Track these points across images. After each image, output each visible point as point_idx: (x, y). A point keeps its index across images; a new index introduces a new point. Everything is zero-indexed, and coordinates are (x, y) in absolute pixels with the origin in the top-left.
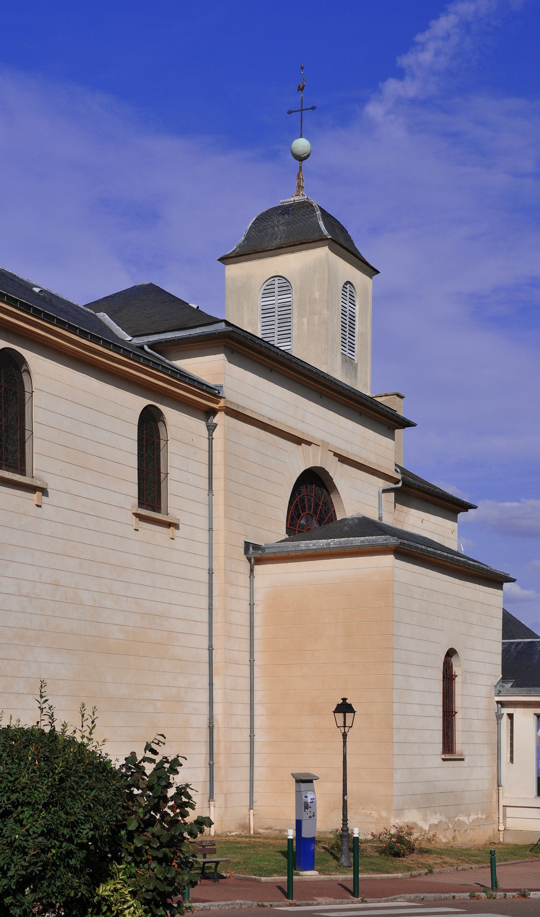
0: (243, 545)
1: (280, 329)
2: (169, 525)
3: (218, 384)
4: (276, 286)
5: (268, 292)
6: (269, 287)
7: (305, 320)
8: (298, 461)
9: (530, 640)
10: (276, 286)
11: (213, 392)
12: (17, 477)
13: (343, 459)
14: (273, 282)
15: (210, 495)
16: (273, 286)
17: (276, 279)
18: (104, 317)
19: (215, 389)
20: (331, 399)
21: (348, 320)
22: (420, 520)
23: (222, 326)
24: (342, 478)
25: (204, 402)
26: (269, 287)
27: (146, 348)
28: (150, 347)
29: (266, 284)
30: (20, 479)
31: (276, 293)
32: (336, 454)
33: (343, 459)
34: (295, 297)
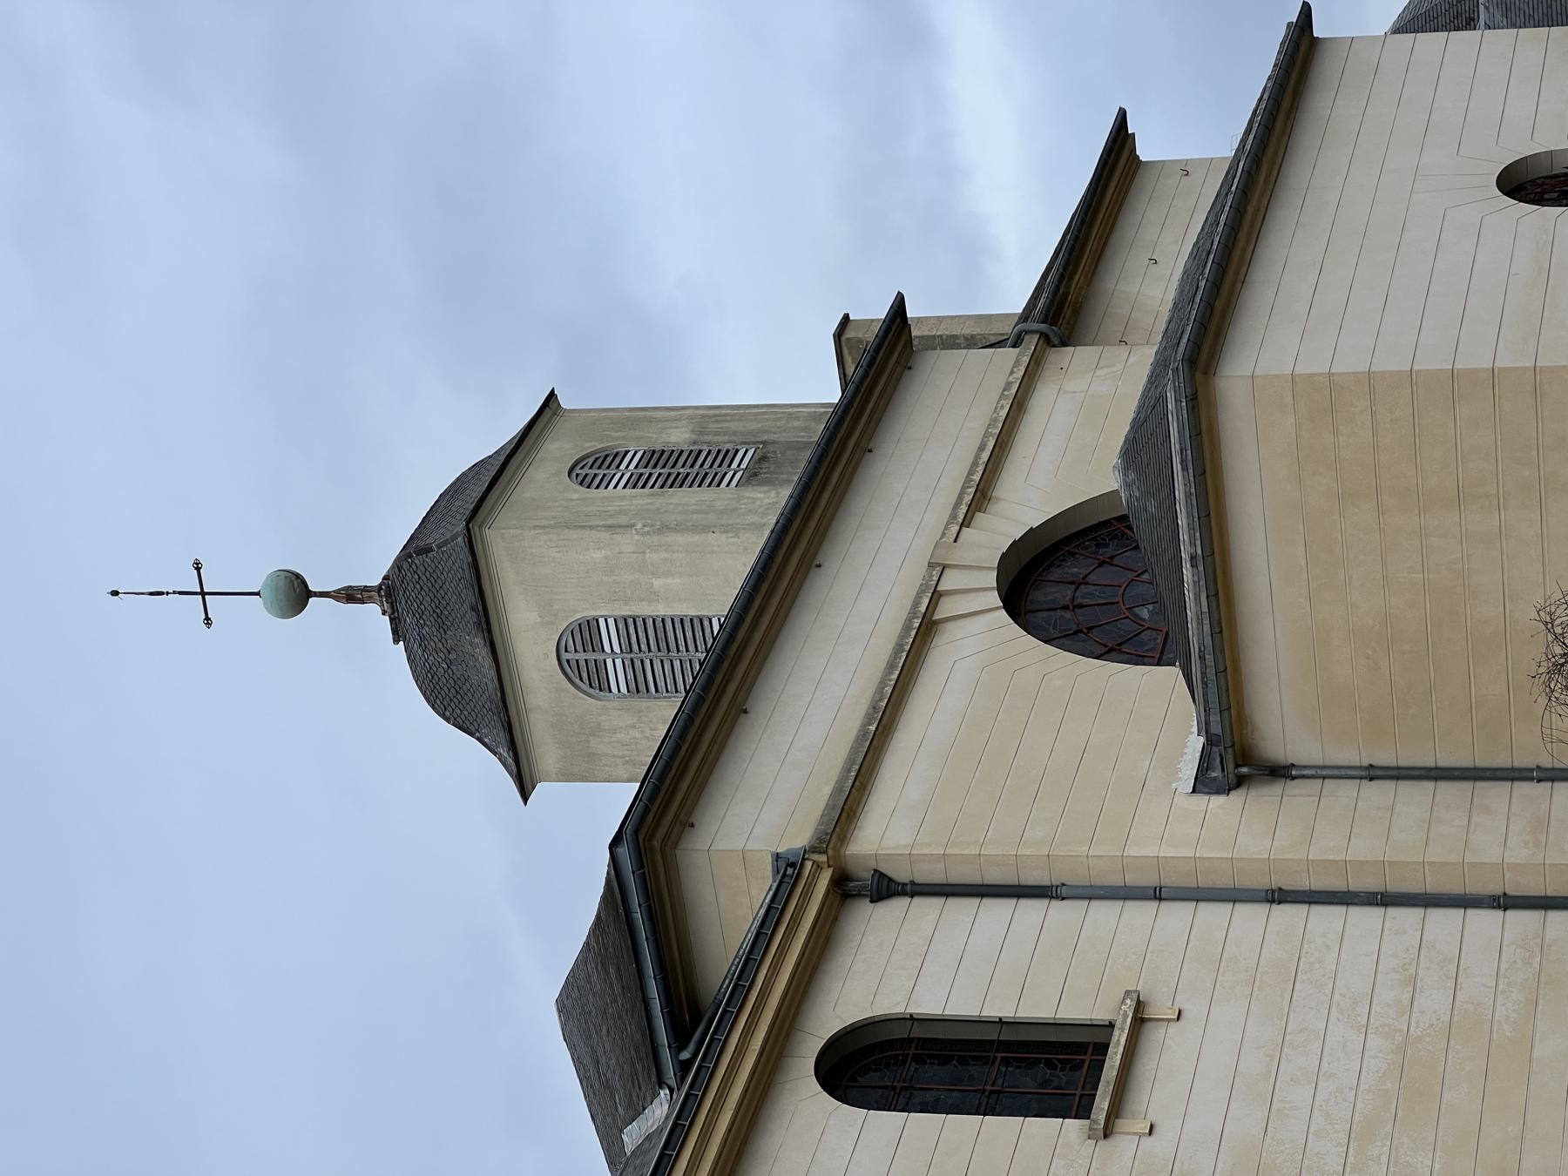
0: (1201, 800)
1: (682, 648)
2: (1140, 1021)
3: (770, 868)
4: (581, 656)
5: (593, 679)
6: (585, 675)
7: (658, 583)
8: (982, 636)
9: (1177, 467)
10: (581, 656)
11: (789, 870)
12: (1120, 1039)
13: (980, 496)
14: (573, 664)
15: (1064, 891)
16: (582, 664)
17: (565, 656)
18: (632, 1136)
19: (784, 875)
20: (822, 535)
21: (658, 471)
22: (1153, 268)
23: (623, 851)
24: (1033, 498)
25: (835, 884)
26: (585, 675)
27: (685, 1055)
28: (681, 1048)
29: (577, 681)
30: (1112, 1067)
31: (600, 657)
32: (966, 523)
33: (980, 496)
34: (606, 610)
